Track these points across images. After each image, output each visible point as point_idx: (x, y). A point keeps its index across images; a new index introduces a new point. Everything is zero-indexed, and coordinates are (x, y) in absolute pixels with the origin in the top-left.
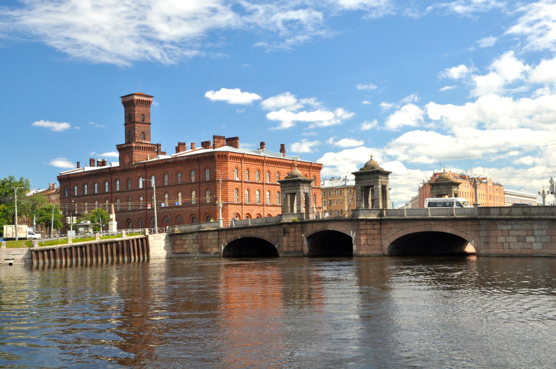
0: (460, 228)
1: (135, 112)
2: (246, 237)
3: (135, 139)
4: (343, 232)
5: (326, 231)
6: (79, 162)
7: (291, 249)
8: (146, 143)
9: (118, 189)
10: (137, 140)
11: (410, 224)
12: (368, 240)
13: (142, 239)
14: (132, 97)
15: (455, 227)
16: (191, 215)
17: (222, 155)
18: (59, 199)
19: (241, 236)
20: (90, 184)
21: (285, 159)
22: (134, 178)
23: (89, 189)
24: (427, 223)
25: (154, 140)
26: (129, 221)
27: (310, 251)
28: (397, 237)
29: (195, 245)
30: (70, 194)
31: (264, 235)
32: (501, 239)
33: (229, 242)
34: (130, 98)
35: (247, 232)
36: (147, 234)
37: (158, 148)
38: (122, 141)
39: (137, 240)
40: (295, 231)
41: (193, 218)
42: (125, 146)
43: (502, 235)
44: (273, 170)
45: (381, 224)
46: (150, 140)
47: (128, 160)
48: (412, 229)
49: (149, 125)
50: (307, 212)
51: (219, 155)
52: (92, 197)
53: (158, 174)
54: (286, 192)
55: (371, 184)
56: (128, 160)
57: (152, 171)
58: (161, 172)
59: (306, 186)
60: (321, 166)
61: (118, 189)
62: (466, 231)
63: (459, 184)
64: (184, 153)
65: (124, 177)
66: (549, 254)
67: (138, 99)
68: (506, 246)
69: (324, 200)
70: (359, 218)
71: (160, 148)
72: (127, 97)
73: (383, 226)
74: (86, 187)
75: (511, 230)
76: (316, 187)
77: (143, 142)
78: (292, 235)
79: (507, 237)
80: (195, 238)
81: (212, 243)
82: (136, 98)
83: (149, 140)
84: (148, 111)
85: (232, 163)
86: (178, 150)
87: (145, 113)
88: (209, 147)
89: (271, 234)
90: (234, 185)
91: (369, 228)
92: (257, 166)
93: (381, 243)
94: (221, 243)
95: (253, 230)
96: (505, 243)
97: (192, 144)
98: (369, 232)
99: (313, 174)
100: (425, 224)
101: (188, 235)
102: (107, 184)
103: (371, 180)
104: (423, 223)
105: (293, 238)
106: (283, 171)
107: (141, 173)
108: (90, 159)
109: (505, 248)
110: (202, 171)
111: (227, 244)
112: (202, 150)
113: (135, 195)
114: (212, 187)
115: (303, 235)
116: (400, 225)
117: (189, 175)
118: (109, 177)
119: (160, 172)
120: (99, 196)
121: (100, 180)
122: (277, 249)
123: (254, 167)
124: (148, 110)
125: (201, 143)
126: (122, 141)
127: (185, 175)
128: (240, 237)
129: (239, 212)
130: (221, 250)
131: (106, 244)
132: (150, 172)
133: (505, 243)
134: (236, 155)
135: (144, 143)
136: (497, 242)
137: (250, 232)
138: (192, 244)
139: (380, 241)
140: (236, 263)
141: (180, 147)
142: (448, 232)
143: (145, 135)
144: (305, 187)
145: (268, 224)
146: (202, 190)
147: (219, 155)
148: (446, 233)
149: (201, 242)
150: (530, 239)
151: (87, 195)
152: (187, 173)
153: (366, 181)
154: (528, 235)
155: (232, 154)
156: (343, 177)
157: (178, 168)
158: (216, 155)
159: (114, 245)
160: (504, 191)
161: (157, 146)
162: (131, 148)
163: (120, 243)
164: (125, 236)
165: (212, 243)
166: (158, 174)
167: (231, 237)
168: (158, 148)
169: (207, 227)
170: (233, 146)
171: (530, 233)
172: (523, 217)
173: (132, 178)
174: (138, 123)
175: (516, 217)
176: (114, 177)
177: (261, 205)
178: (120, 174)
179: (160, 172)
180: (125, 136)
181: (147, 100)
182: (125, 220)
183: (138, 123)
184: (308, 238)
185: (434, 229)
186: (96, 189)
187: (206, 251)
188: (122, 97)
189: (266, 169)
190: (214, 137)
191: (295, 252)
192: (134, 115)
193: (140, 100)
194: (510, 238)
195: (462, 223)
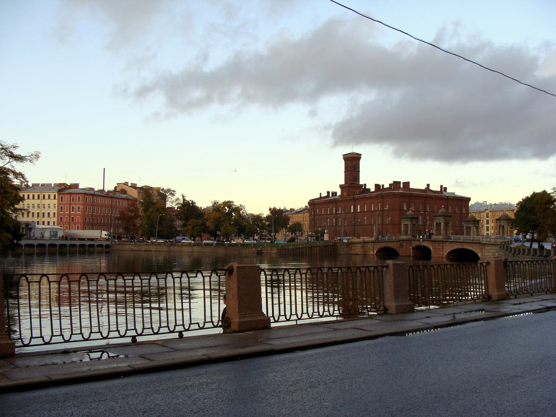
9: (359, 211)
24: (462, 244)
28: (449, 251)
29: (361, 250)
40: (406, 245)
45: (443, 243)
46: (359, 181)
69: (492, 219)
73: (444, 244)
74: (366, 206)
78: (405, 247)
98: (437, 247)
115: (411, 247)
120: (330, 216)
141: (377, 186)
145: (396, 240)
148: (469, 250)
151: (323, 215)
160: (427, 238)
172: (494, 243)
175: (492, 243)
186: (328, 212)
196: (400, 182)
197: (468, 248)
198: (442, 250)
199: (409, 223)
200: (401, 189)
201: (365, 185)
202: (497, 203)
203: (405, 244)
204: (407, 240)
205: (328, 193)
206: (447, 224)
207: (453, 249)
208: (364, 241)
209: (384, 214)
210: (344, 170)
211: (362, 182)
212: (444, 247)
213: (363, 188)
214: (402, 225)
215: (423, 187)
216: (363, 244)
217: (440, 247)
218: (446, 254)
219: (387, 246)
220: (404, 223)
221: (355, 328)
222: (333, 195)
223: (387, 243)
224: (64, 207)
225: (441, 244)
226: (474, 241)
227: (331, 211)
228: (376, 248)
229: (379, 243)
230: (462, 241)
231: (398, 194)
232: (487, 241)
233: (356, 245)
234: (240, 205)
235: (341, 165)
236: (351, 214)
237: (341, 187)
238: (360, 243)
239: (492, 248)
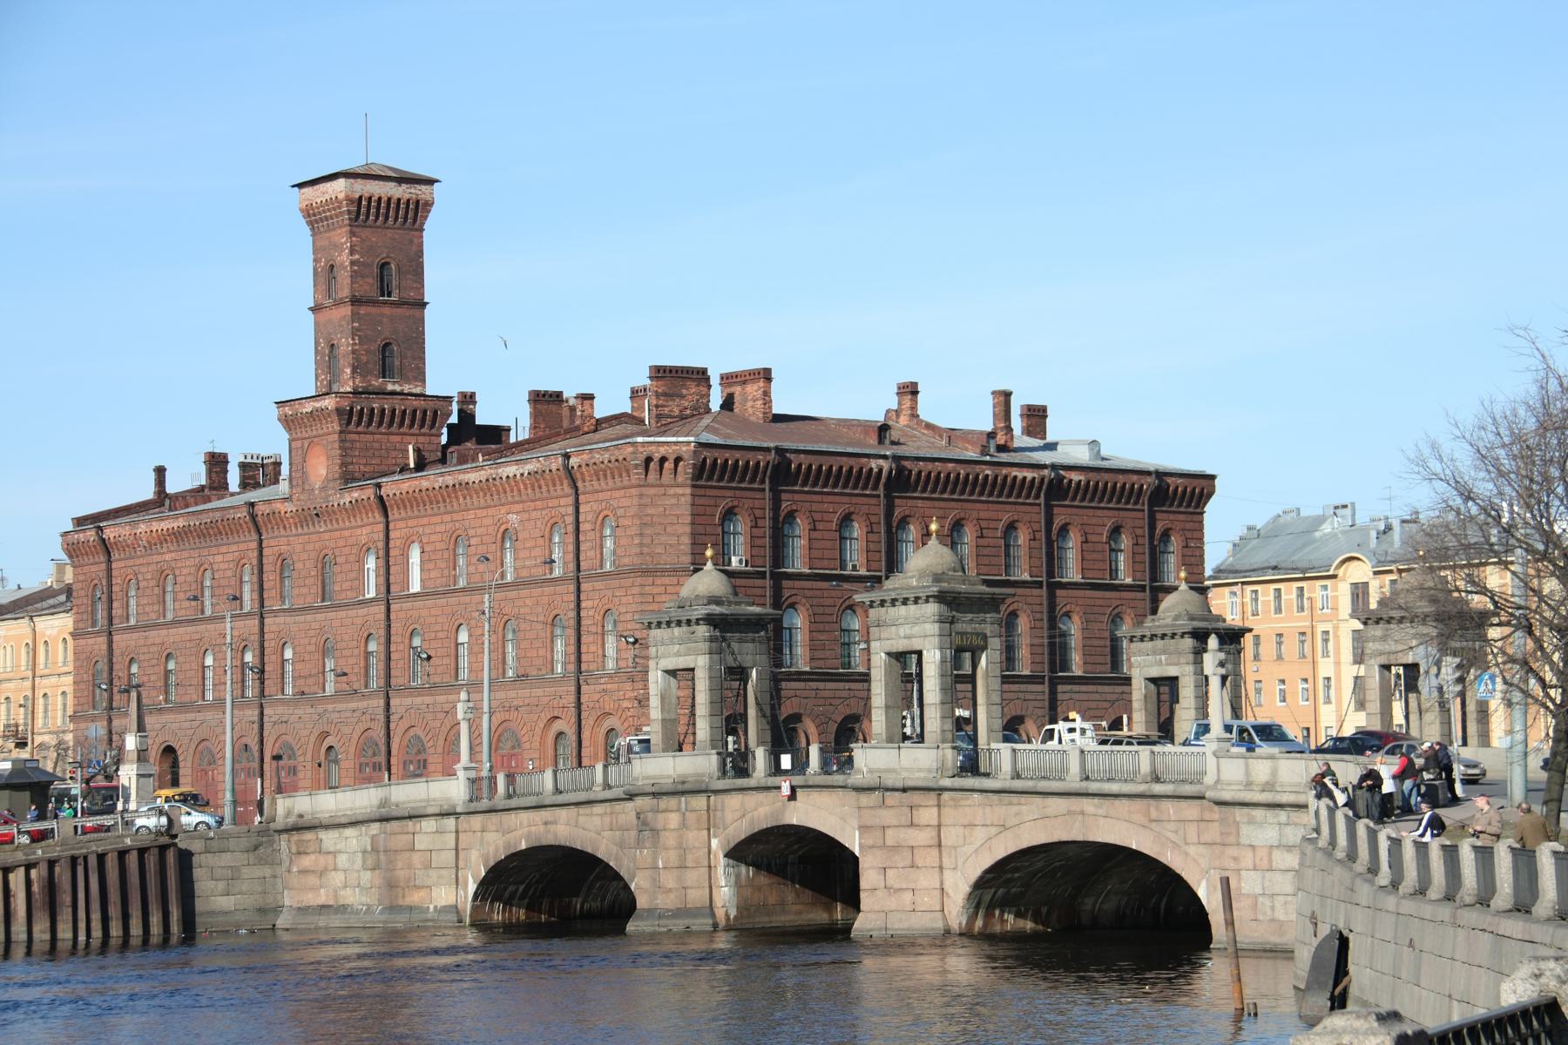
2: (545, 842)
5: (783, 826)
7: (667, 902)
8: (401, 393)
9: (415, 587)
12: (890, 873)
15: (1154, 825)
18: (69, 639)
19: (528, 837)
20: (185, 571)
22: (346, 551)
25: (441, 379)
28: (987, 861)
29: (367, 876)
33: (492, 863)
40: (684, 825)
42: (308, 407)
43: (1251, 867)
46: (420, 376)
52: (190, 629)
57: (410, 523)
58: (441, 528)
59: (741, 641)
61: (415, 587)
62: (1187, 844)
65: (309, 547)
66: (908, 930)
67: (361, 197)
75: (1278, 847)
77: (390, 387)
78: (669, 839)
79: (1268, 874)
80: (369, 848)
83: (416, 379)
84: (414, 248)
89: (618, 833)
91: (894, 822)
93: (942, 883)
96: (1261, 899)
105: (673, 856)
108: (531, 393)
109: (1261, 918)
111: (484, 874)
113: (440, 620)
114: (624, 600)
115: (715, 843)
117: (541, 541)
119: (438, 529)
124: (411, 242)
125: (629, 394)
133: (1261, 899)
135: (393, 393)
138: (358, 871)
139: (937, 875)
142: (1134, 847)
149: (390, 862)
152: (537, 533)
173: (471, 532)
178: (294, 531)
181: (407, 196)
182: (313, 739)
191: (679, 913)
196: (704, 371)
198: (935, 852)
200: (707, 420)
201: (468, 399)
202: (1048, 420)
203: (673, 819)
204: (682, 790)
205: (217, 462)
206: (962, 652)
207: (1012, 848)
208: (384, 803)
210: (433, 318)
211: (441, 379)
212: (950, 836)
213: (454, 419)
214: (656, 679)
215: (874, 405)
216: (375, 828)
217: (923, 837)
218: (965, 888)
219: (549, 840)
220: (671, 663)
221: (1239, 980)
222: (247, 483)
224: (1336, 628)
225: (927, 815)
226: (1158, 788)
229: (494, 818)
230: (1073, 780)
231: (535, 428)
232: (1249, 785)
233: (329, 838)
235: (152, 476)
236: (363, 611)
237: (293, 417)
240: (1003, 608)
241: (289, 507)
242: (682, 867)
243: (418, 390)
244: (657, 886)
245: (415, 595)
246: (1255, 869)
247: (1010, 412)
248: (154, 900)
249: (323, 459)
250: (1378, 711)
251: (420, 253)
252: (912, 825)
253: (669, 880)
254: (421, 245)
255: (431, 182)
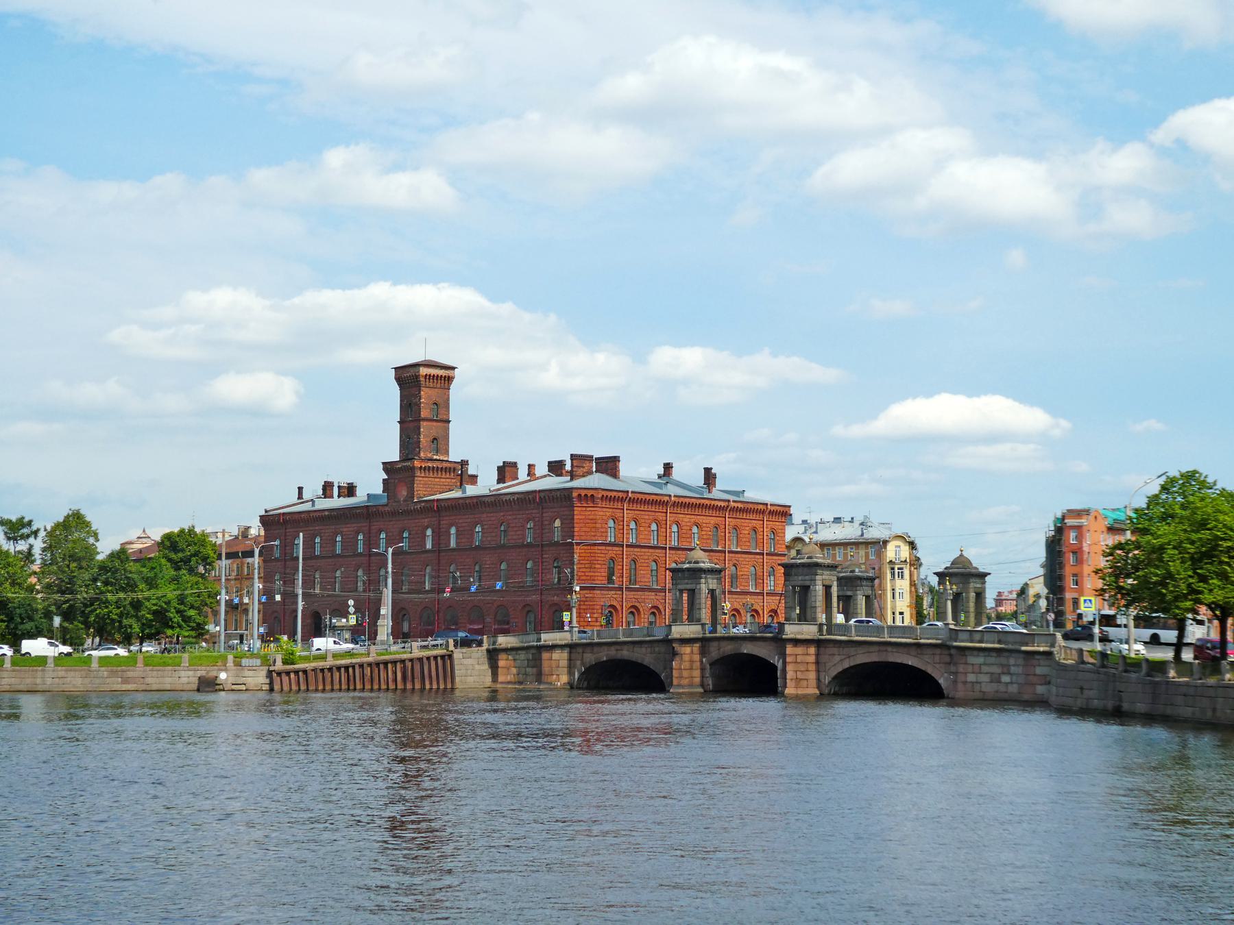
0: (926, 658)
1: (420, 399)
3: (419, 453)
4: (763, 657)
6: (302, 488)
8: (439, 460)
9: (453, 544)
10: (422, 455)
11: (861, 650)
13: (443, 657)
14: (415, 369)
16: (525, 606)
17: (586, 495)
19: (607, 655)
20: (327, 534)
21: (711, 499)
23: (324, 545)
24: (883, 648)
25: (455, 455)
26: (403, 612)
27: (714, 685)
29: (529, 670)
30: (285, 554)
31: (646, 657)
32: (971, 678)
33: (588, 666)
34: (412, 371)
35: (617, 650)
36: (451, 648)
37: (462, 468)
38: (395, 456)
39: (435, 658)
41: (529, 612)
44: (686, 520)
46: (447, 452)
47: (405, 493)
48: (862, 658)
49: (446, 425)
50: (714, 622)
51: (580, 495)
53: (464, 524)
54: (680, 587)
55: (807, 583)
56: (405, 494)
60: (787, 509)
63: (986, 576)
64: (514, 485)
68: (977, 687)
70: (784, 636)
71: (467, 469)
72: (407, 369)
74: (318, 540)
76: (739, 550)
77: (435, 457)
78: (686, 658)
80: (531, 658)
81: (558, 667)
82: (424, 371)
85: (605, 510)
86: (501, 480)
87: (440, 401)
88: (564, 472)
90: (606, 552)
92: (653, 514)
94: (575, 667)
95: (626, 647)
97: (530, 466)
98: (799, 659)
99: (769, 527)
100: (879, 651)
101: (520, 652)
102: (360, 537)
103: (807, 577)
104: (876, 648)
106: (707, 521)
107: (429, 519)
110: (546, 523)
112: (548, 478)
116: (846, 650)
118: (364, 524)
121: (348, 528)
122: (665, 681)
123: (646, 514)
126: (395, 456)
127: (515, 529)
128: (605, 659)
129: (615, 603)
130: (574, 679)
131: (386, 663)
132: (447, 518)
134: (613, 494)
136: (821, 694)
137: (622, 650)
140: (622, 697)
141: (506, 471)
143: (440, 443)
144: (710, 581)
146: (548, 560)
147: (580, 495)
150: (1006, 679)
153: (800, 578)
154: (1003, 673)
155: (605, 493)
156: (859, 519)
157: (502, 514)
158: (575, 494)
159: (399, 665)
161: (462, 465)
162: (413, 469)
163: (409, 664)
164: (415, 649)
165: (558, 667)
166: (464, 524)
167: (590, 658)
168: (462, 468)
169: (548, 638)
170: (608, 474)
171: (1005, 670)
174: (424, 420)
176: (375, 523)
177: (660, 591)
179: (466, 521)
180: (400, 445)
181: (444, 375)
183: (424, 420)
184: (711, 665)
185: (891, 659)
187: (549, 681)
188: (395, 368)
189: (672, 519)
190: (573, 457)
192: (418, 405)
193: (430, 375)
194: (981, 675)
195: (929, 651)
196: (592, 457)
197: (905, 662)
199: (972, 585)
201: (464, 463)
209: (862, 552)
210: (397, 416)
223: (618, 647)
227: (350, 543)
228: (579, 663)
234: (266, 511)
236: (426, 555)
238: (562, 647)
239: (991, 660)
240: (1201, 584)
241: (387, 509)
242: (691, 669)
243: (446, 459)
244: (681, 677)
245: (453, 550)
246: (973, 673)
247: (582, 456)
248: (203, 697)
249: (405, 488)
250: (499, 669)
251: (448, 399)
252: (807, 654)
253: (685, 674)
254: (449, 395)
255: (453, 368)
